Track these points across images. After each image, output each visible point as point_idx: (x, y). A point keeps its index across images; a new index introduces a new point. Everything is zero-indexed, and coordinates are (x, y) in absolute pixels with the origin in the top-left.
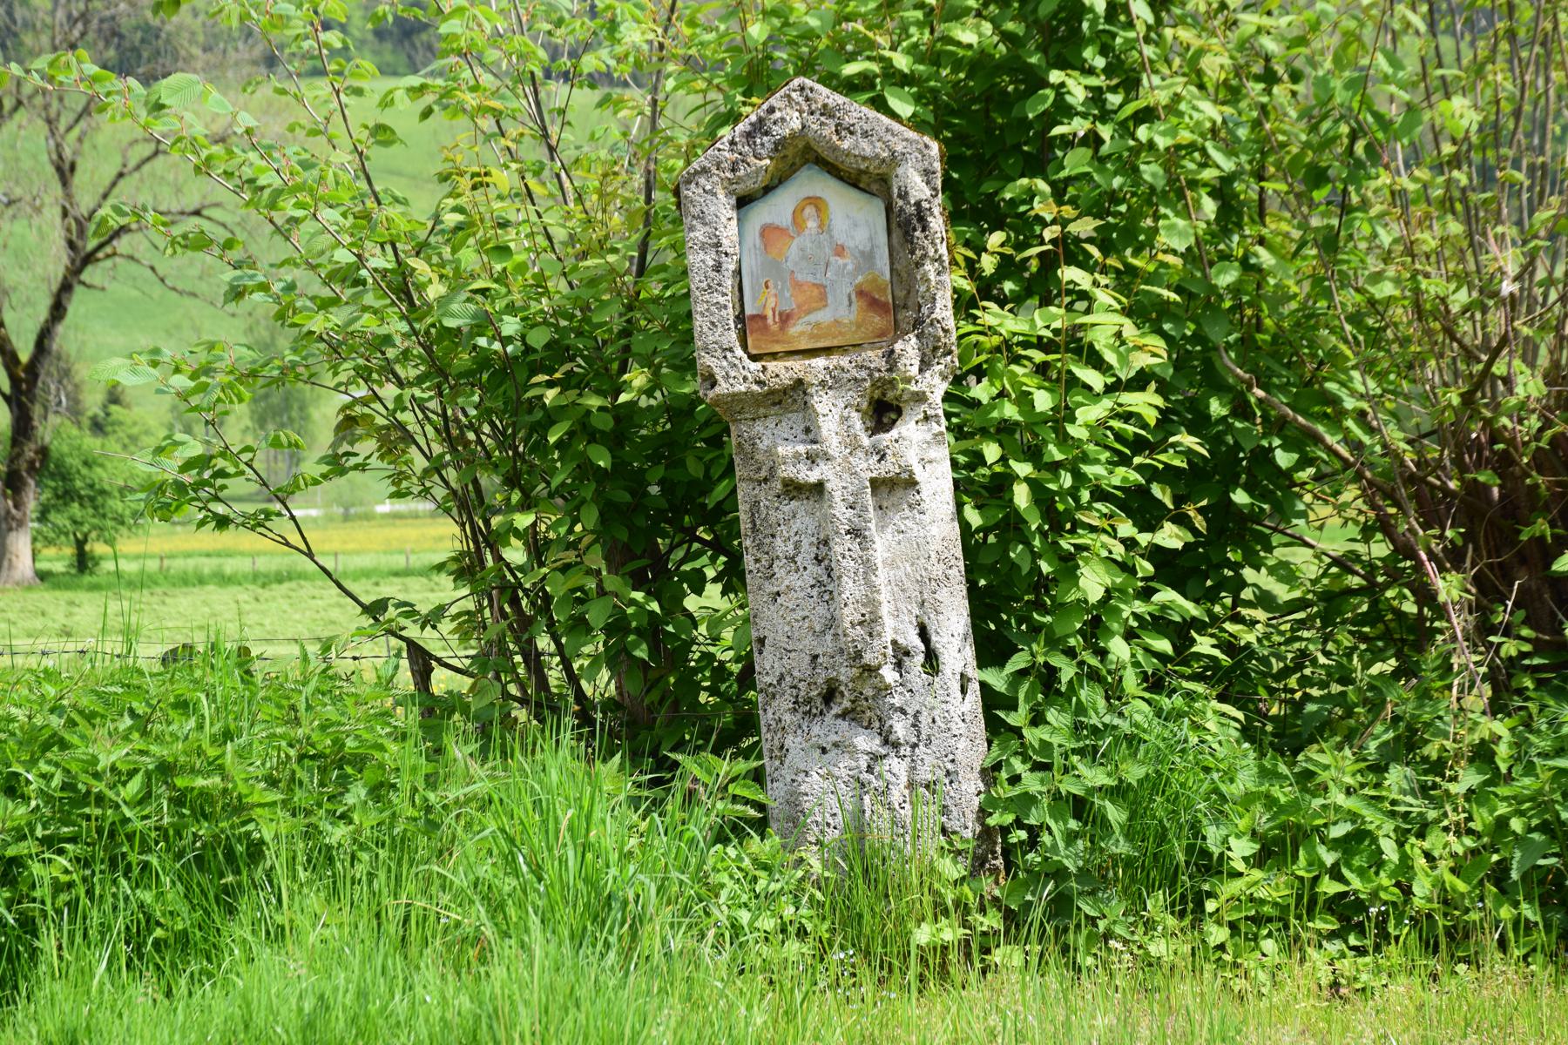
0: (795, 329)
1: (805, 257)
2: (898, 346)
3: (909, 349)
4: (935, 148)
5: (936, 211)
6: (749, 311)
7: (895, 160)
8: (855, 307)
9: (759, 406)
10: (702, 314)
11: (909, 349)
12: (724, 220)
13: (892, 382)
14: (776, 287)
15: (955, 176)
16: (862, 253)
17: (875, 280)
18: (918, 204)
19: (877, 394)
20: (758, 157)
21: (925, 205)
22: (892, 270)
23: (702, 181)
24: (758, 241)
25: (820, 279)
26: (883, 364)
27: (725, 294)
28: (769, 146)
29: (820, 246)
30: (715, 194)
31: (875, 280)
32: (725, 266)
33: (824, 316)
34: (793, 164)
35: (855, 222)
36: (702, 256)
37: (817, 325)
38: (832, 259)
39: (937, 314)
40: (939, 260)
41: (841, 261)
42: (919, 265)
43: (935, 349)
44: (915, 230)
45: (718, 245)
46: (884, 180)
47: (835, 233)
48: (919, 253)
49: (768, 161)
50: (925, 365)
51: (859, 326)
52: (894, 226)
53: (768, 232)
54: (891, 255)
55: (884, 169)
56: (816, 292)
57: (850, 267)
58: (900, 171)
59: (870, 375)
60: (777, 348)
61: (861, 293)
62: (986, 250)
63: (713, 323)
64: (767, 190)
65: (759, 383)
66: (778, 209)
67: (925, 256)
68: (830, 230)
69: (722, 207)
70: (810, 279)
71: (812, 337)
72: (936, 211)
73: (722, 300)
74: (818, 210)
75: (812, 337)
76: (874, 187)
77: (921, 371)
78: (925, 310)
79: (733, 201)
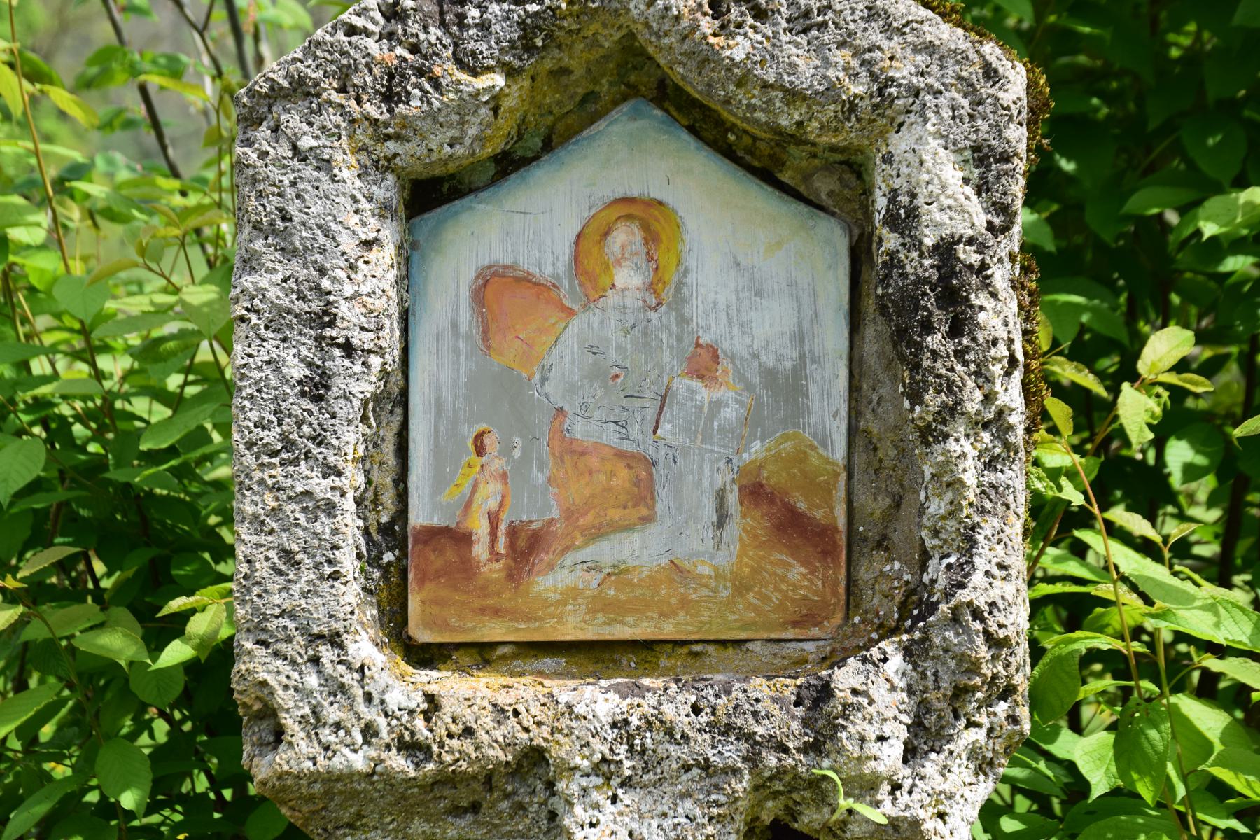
0: (550, 581)
1: (604, 376)
2: (846, 678)
3: (879, 689)
4: (1016, 82)
5: (1001, 276)
6: (419, 517)
7: (887, 106)
8: (733, 529)
9: (409, 814)
10: (258, 524)
11: (879, 691)
12: (348, 243)
13: (818, 786)
14: (506, 451)
15: (1068, 166)
16: (770, 375)
17: (800, 457)
18: (945, 249)
19: (770, 811)
20: (469, 64)
21: (968, 255)
22: (852, 432)
23: (292, 120)
24: (465, 316)
25: (637, 439)
26: (791, 727)
27: (332, 471)
28: (505, 32)
29: (646, 343)
30: (325, 165)
31: (800, 457)
32: (338, 384)
33: (641, 550)
34: (590, 97)
35: (759, 280)
36: (271, 348)
37: (619, 572)
38: (682, 385)
39: (977, 591)
40: (998, 423)
41: (705, 394)
42: (931, 435)
43: (961, 692)
44: (928, 328)
45: (326, 318)
46: (853, 168)
47: (696, 310)
48: (933, 400)
49: (498, 80)
50: (924, 738)
51: (741, 588)
52: (870, 306)
53: (496, 287)
54: (854, 388)
55: (850, 134)
56: (623, 476)
57: (730, 413)
58: (900, 143)
59: (753, 759)
60: (493, 631)
61: (755, 492)
62: (1134, 377)
63: (287, 555)
64: (508, 165)
65: (411, 747)
66: (534, 223)
67: (952, 411)
68: (679, 301)
69: (350, 212)
70: (609, 435)
71: (601, 606)
72: (1001, 276)
73: (321, 486)
74: (651, 237)
75: (601, 606)
76: (824, 186)
77: (911, 754)
78: (937, 571)
79: (386, 190)
